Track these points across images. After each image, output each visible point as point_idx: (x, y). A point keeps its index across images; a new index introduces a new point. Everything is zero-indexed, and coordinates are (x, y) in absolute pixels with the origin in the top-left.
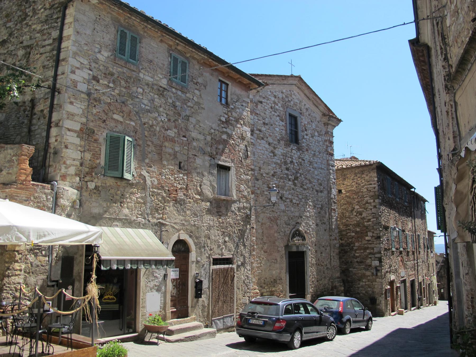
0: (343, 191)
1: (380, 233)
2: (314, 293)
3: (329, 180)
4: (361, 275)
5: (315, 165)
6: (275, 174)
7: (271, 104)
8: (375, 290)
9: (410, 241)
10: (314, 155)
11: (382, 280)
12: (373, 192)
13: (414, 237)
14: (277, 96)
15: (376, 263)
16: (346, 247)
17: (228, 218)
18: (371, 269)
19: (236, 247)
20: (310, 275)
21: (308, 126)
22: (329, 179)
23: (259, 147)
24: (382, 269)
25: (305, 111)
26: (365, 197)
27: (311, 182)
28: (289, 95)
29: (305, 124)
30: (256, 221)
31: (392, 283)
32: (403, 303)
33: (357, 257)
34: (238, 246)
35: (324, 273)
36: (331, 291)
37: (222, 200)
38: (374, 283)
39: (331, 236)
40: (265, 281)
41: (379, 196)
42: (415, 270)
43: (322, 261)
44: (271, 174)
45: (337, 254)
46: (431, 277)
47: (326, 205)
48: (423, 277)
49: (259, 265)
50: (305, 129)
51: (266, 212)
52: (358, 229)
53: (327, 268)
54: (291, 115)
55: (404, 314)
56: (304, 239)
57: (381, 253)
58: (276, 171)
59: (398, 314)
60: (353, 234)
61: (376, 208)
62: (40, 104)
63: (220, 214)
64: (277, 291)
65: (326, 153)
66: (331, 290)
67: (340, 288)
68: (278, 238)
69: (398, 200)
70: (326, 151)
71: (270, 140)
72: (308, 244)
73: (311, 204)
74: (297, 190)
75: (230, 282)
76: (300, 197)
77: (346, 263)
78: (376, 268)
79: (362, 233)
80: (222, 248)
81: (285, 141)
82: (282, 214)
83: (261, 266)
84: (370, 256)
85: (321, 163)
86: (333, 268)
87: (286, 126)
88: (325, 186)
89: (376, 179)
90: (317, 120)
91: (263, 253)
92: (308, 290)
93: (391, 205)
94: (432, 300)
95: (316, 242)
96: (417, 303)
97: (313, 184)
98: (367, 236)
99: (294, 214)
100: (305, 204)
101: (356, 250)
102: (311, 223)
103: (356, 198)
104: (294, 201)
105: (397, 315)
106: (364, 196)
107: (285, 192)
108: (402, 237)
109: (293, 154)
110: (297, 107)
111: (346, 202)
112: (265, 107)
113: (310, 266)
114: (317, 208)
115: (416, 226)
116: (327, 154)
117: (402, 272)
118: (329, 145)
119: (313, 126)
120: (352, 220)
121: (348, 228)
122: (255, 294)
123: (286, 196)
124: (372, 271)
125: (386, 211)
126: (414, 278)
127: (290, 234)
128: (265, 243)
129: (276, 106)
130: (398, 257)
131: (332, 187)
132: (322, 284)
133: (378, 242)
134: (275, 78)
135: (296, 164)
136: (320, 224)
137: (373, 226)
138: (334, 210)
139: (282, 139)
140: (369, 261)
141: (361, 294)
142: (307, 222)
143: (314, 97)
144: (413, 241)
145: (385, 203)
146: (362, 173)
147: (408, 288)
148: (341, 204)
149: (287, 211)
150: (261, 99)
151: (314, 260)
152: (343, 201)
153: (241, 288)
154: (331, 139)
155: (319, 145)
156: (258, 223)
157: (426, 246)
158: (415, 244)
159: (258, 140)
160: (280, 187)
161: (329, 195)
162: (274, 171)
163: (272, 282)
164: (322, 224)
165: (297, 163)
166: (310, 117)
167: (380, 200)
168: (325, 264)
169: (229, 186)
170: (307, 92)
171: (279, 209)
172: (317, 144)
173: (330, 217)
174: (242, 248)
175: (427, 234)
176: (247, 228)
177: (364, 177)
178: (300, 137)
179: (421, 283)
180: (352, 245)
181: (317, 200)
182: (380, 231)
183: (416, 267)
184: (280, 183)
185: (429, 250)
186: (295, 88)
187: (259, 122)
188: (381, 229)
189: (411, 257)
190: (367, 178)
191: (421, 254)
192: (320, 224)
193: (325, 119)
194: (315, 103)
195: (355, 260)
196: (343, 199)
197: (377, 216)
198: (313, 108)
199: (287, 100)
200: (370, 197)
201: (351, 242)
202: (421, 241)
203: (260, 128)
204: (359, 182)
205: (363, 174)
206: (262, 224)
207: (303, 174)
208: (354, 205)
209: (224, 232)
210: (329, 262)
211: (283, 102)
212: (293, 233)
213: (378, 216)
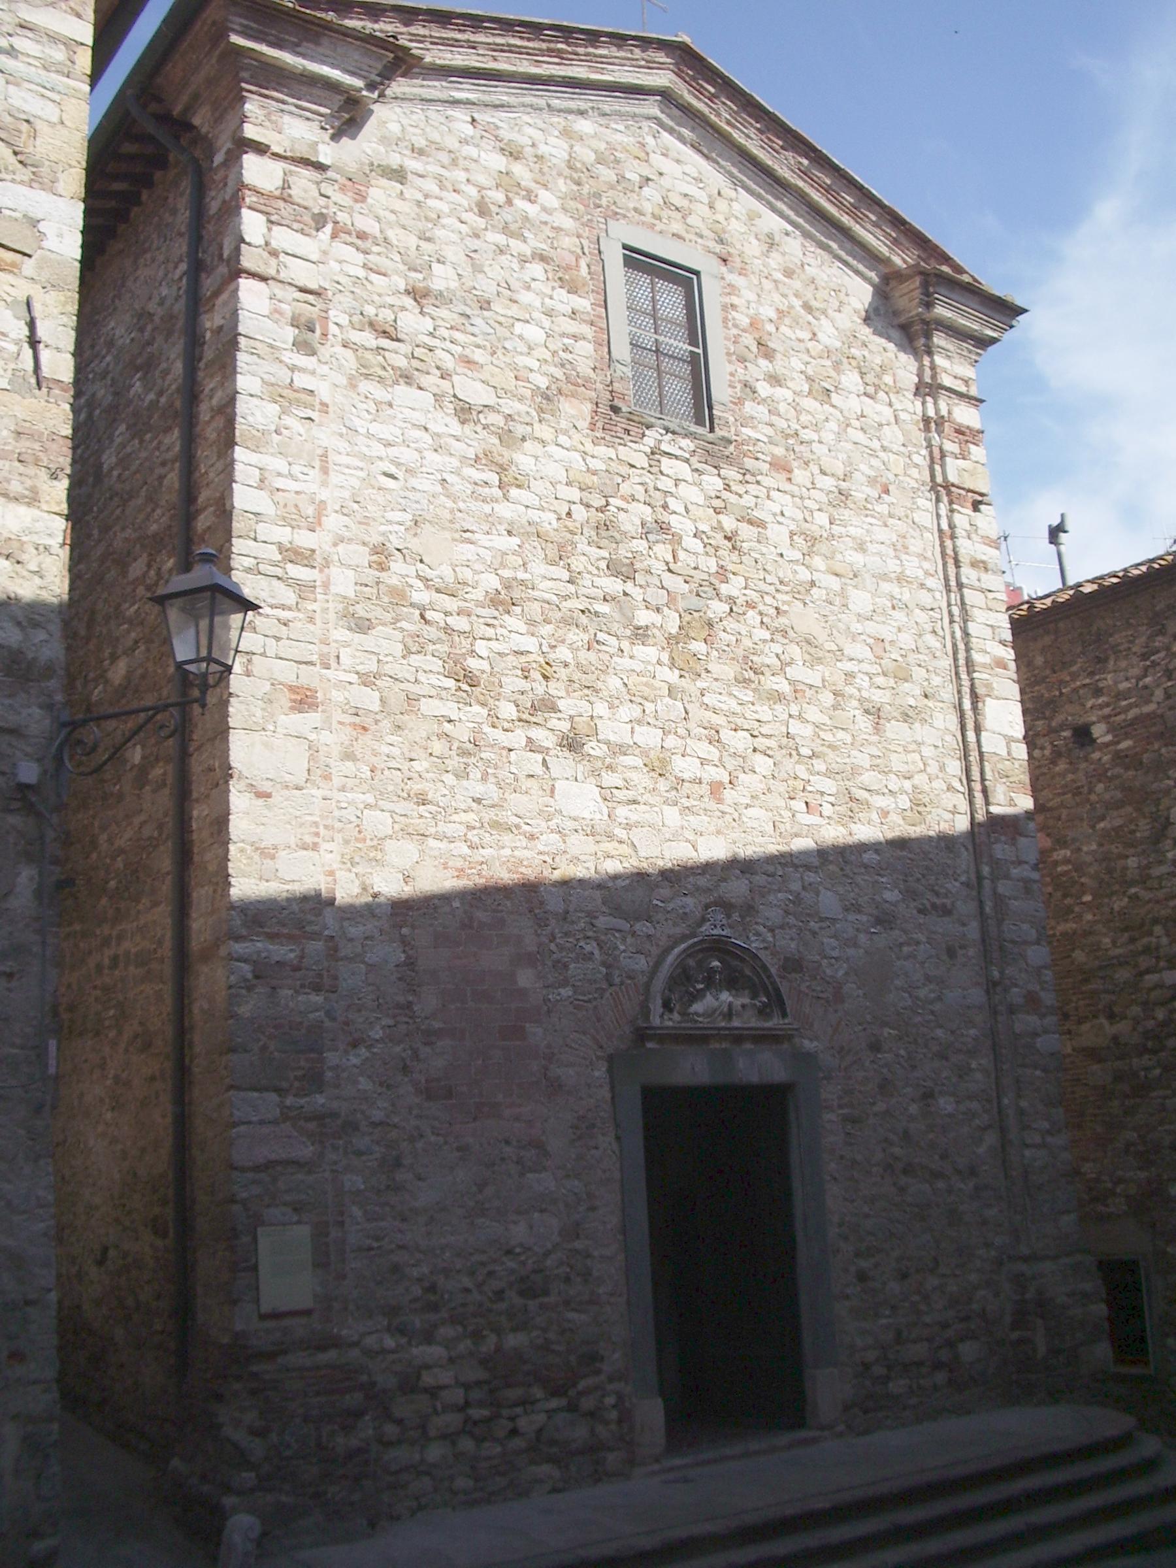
5: (858, 559)
14: (528, 151)
21: (783, 329)
23: (375, 428)
25: (753, 248)
29: (754, 324)
36: (1015, 1335)
44: (478, 594)
51: (442, 827)
58: (521, 575)
62: (135, 560)
85: (900, 548)
104: (684, 767)
107: (601, 709)
109: (666, 484)
111: (1119, 795)
119: (820, 335)
120: (1161, 894)
123: (614, 728)
129: (520, 203)
139: (574, 384)
148: (1094, 809)
150: (394, 160)
152: (1100, 787)
155: (876, 444)
159: (365, 386)
162: (506, 573)
166: (797, 284)
172: (860, 437)
173: (986, 870)
178: (720, 391)
187: (374, 277)
203: (387, 315)
207: (750, 605)
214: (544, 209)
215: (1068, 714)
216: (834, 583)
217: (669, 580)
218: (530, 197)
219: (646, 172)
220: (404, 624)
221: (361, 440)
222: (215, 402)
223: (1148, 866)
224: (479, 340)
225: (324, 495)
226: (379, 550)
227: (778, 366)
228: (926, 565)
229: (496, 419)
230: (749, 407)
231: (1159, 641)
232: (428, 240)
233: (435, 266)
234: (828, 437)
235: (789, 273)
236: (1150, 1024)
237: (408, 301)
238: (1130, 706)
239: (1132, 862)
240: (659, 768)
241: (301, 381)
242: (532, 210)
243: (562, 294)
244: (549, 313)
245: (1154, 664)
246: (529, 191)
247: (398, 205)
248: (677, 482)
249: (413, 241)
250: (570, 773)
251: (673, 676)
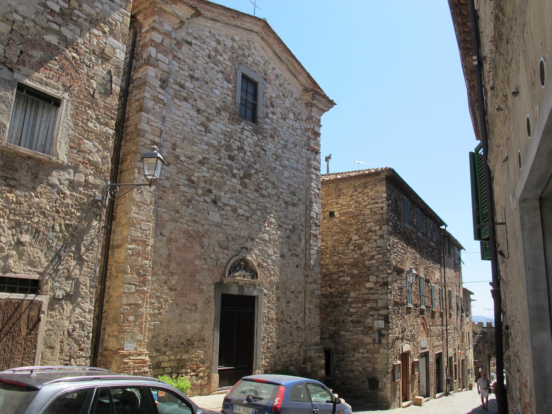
0: (336, 214)
1: (387, 278)
2: (269, 368)
3: (308, 189)
4: (357, 342)
5: (286, 163)
6: (206, 161)
7: (210, 51)
8: (377, 366)
9: (436, 296)
10: (285, 146)
11: (388, 351)
12: (379, 214)
13: (443, 293)
14: (222, 43)
15: (380, 324)
16: (337, 298)
17: (37, 197)
18: (372, 333)
19: (54, 258)
20: (264, 337)
21: (277, 100)
22: (309, 187)
23: (177, 112)
24: (389, 333)
25: (273, 77)
26: (367, 223)
27: (275, 187)
28: (246, 46)
30: (155, 232)
31: (405, 356)
32: (423, 386)
33: (352, 314)
34: (60, 257)
35: (291, 335)
36: (302, 366)
37: (22, 157)
38: (376, 355)
39: (307, 276)
40: (167, 340)
41: (388, 220)
42: (442, 340)
43: (288, 315)
44: (196, 160)
45: (316, 307)
46: (466, 351)
47: (301, 228)
48: (455, 351)
49: (156, 311)
50: (271, 103)
51: (181, 220)
52: (355, 272)
53: (298, 328)
54: (245, 77)
55: (424, 404)
56: (254, 275)
57: (389, 309)
58: (207, 156)
59: (415, 404)
60: (348, 279)
61: (384, 238)
63: (12, 183)
64: (192, 360)
65: (307, 147)
66: (303, 364)
67: (318, 361)
68: (202, 269)
69: (420, 235)
70: (307, 144)
71: (201, 105)
72: (263, 285)
73: (273, 220)
74: (248, 195)
75: (24, 331)
76: (254, 207)
77: (336, 323)
78: (379, 331)
79: (360, 277)
80: (8, 257)
81: (230, 113)
82: (213, 228)
83: (160, 314)
84: (371, 313)
85: (297, 162)
86: (308, 328)
87: (234, 91)
88: (302, 197)
89: (385, 195)
90: (295, 96)
91: (167, 291)
92: (258, 361)
93: (409, 240)
94: (467, 383)
95: (278, 283)
96: (444, 388)
97: (280, 190)
98: (368, 281)
99: (237, 233)
100: (262, 220)
101: (352, 303)
102: (271, 252)
103: (354, 225)
104: (240, 211)
105: (412, 406)
106: (365, 220)
107: (222, 194)
108: (425, 289)
109: (243, 137)
110: (259, 68)
112: (197, 53)
113: (264, 322)
114: (284, 230)
115: (446, 278)
116: (308, 150)
117: (424, 341)
118: (312, 137)
119: (286, 103)
120: (347, 257)
121: (341, 269)
122: (139, 363)
123: (224, 200)
124: (374, 335)
125: (400, 246)
126: (441, 351)
127: (227, 264)
128: (172, 273)
129: (219, 57)
130: (418, 318)
131: (314, 199)
132: (286, 352)
133: (384, 291)
134: (216, 10)
135: (248, 153)
136: (289, 255)
137: (378, 267)
138: (315, 236)
139: (225, 108)
140: (369, 320)
141: (356, 372)
142: (263, 250)
143: (290, 58)
144: (441, 299)
145: (399, 233)
146: (365, 186)
147: (432, 365)
149: (226, 225)
150: (189, 39)
151: (272, 312)
153: (58, 347)
154: (316, 129)
155: (295, 133)
156: (160, 237)
157: (460, 309)
158: (444, 303)
159: (175, 100)
160: (214, 184)
161: (308, 212)
162: (204, 156)
163: (182, 344)
164: (292, 255)
165: (250, 151)
166: (282, 89)
167: (390, 228)
168: (294, 320)
169: (52, 138)
170: (277, 47)
171: (208, 220)
172: (291, 131)
173: (308, 247)
174: (73, 263)
175: (461, 291)
176: (89, 227)
177: (367, 193)
179: (451, 358)
180: (345, 295)
181: (286, 217)
182: (388, 274)
183: (445, 336)
184: (215, 178)
185: (464, 314)
186: (257, 39)
187: (181, 71)
188: (389, 271)
189: (438, 320)
190: (371, 193)
191: (452, 318)
192: (288, 255)
193: (307, 97)
194: (292, 69)
195: (350, 319)
196: (335, 225)
197: (384, 251)
198: (288, 76)
199: (240, 52)
200: (375, 222)
201: (344, 290)
202: (454, 300)
203: (182, 82)
204: (360, 199)
205: (366, 187)
206: (170, 240)
207: (261, 171)
208: (351, 234)
209: (18, 224)
210: (302, 319)
211: (233, 53)
212: (234, 263)
213: (385, 251)
214: (224, 59)
215: (329, 209)
216: (281, 168)
217: (242, 162)
218: (221, 55)
219: (250, 53)
220: (178, 165)
221: (172, 115)
222: (136, 98)
223: (345, 250)
224: (204, 92)
225: (163, 128)
226: (174, 144)
227: (275, 110)
228: (303, 167)
229: (205, 114)
230: (267, 120)
231: (355, 193)
232: (195, 63)
233: (196, 70)
234: (284, 130)
235: (280, 85)
236: (340, 290)
237: (188, 79)
238: (345, 209)
239: (341, 248)
240: (235, 210)
241: (160, 96)
242: (221, 59)
243: (225, 83)
244: (222, 87)
245: (353, 199)
246: (221, 53)
247: (189, 52)
248: (247, 137)
249: (192, 62)
250: (213, 210)
251: (240, 188)
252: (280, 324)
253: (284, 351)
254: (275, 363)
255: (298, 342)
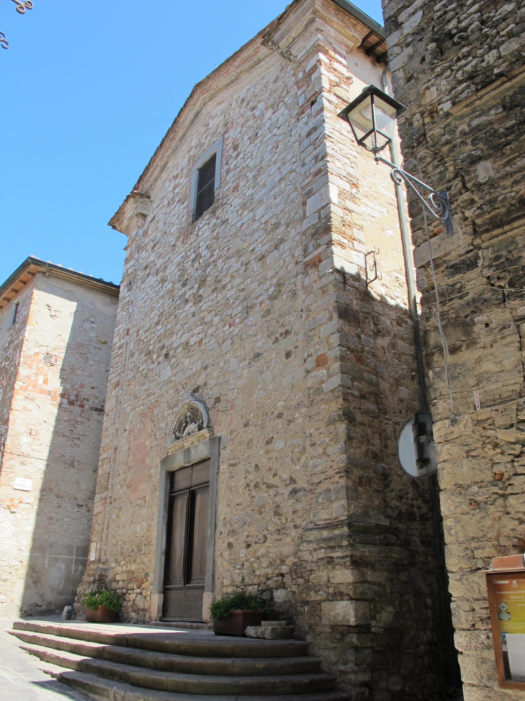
43: (270, 469)
252: (254, 493)
253: (262, 551)
254: (243, 579)
255: (296, 527)
